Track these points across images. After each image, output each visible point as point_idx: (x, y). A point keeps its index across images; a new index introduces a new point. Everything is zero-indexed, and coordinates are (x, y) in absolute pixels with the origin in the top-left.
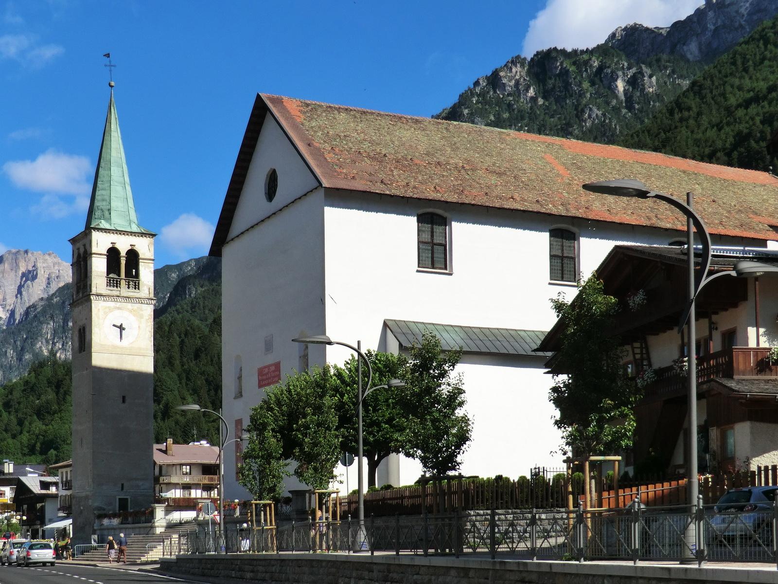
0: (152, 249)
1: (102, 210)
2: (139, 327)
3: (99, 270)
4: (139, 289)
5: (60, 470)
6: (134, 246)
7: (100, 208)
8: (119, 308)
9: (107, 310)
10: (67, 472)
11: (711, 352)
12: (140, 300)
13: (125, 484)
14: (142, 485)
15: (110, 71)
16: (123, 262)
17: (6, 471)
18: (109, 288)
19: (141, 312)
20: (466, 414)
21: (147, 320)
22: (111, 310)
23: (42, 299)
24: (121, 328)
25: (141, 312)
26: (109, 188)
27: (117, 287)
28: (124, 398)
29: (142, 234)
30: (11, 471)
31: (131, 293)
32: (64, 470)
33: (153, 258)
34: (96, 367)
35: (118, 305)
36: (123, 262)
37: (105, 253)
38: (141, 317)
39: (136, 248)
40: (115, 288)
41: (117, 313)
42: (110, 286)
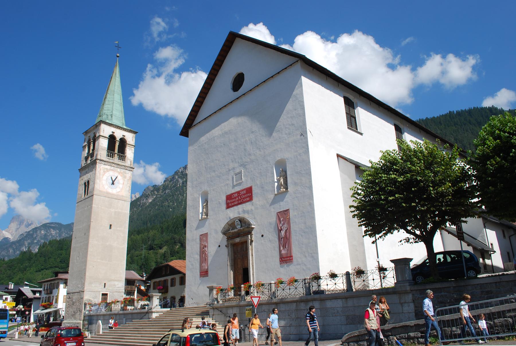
0: (134, 140)
1: (107, 115)
2: (123, 183)
3: (103, 146)
4: (125, 161)
5: (43, 284)
6: (125, 136)
7: (106, 114)
8: (112, 170)
9: (106, 170)
10: (48, 285)
12: (125, 167)
14: (118, 284)
17: (10, 288)
18: (107, 157)
19: (125, 175)
20: (263, 287)
21: (128, 180)
22: (108, 170)
23: (26, 232)
25: (125, 175)
26: (112, 104)
27: (112, 157)
28: (111, 225)
29: (130, 131)
30: (12, 288)
31: (120, 162)
32: (46, 284)
33: (134, 145)
34: (259, 23)
35: (112, 168)
37: (108, 137)
38: (125, 177)
39: (126, 138)
40: (111, 158)
42: (108, 156)
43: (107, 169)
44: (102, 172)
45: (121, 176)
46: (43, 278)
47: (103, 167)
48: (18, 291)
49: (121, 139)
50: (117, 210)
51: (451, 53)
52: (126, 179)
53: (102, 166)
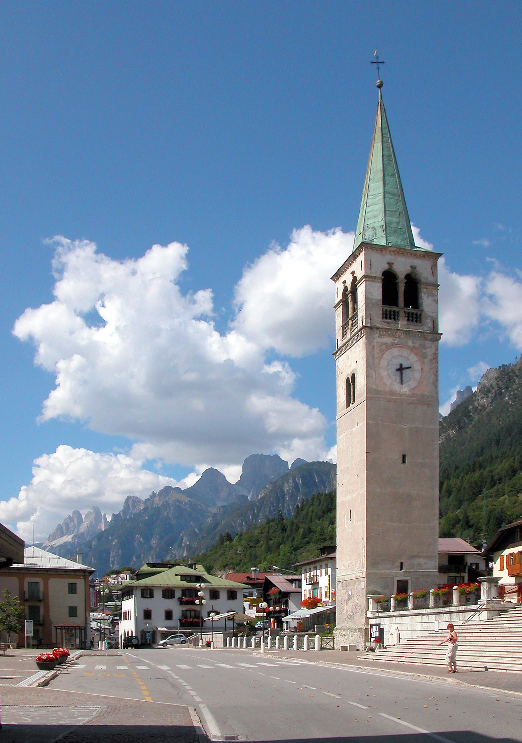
3: (374, 297)
7: (371, 226)
9: (383, 347)
11: (6, 560)
13: (404, 563)
15: (378, 68)
16: (401, 288)
19: (424, 351)
22: (389, 347)
24: (401, 369)
25: (424, 351)
27: (394, 319)
28: (404, 457)
31: (414, 328)
36: (401, 288)
40: (392, 321)
41: (395, 351)
42: (386, 318)
43: (385, 344)
44: (378, 351)
45: (416, 355)
46: (5, 704)
47: (377, 342)
48: (265, 581)
49: (408, 277)
50: (413, 426)
51: (155, 244)
52: (426, 360)
53: (375, 341)
